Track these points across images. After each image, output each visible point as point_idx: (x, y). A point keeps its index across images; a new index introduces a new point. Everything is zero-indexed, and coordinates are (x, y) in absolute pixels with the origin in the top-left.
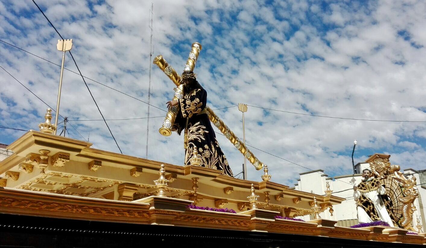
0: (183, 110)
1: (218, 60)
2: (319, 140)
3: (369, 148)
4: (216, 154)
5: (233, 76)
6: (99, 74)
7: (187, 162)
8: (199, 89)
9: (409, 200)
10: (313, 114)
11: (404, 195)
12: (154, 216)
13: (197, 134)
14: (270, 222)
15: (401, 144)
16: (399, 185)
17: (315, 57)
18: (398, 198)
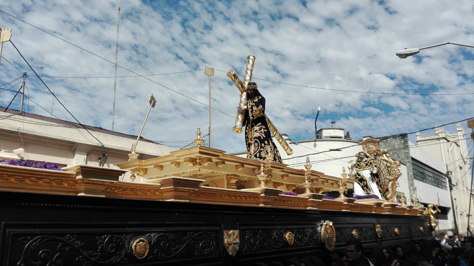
0: (250, 114)
1: (191, 14)
2: (287, 102)
3: (335, 112)
4: (273, 148)
5: (205, 31)
6: (64, 22)
7: (254, 153)
8: (260, 97)
9: (394, 178)
10: (284, 76)
11: (390, 173)
12: (262, 200)
13: (260, 133)
14: (319, 202)
15: (366, 109)
16: (386, 165)
17: (289, 16)
18: (384, 175)
